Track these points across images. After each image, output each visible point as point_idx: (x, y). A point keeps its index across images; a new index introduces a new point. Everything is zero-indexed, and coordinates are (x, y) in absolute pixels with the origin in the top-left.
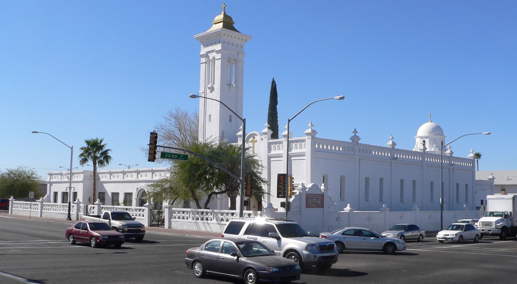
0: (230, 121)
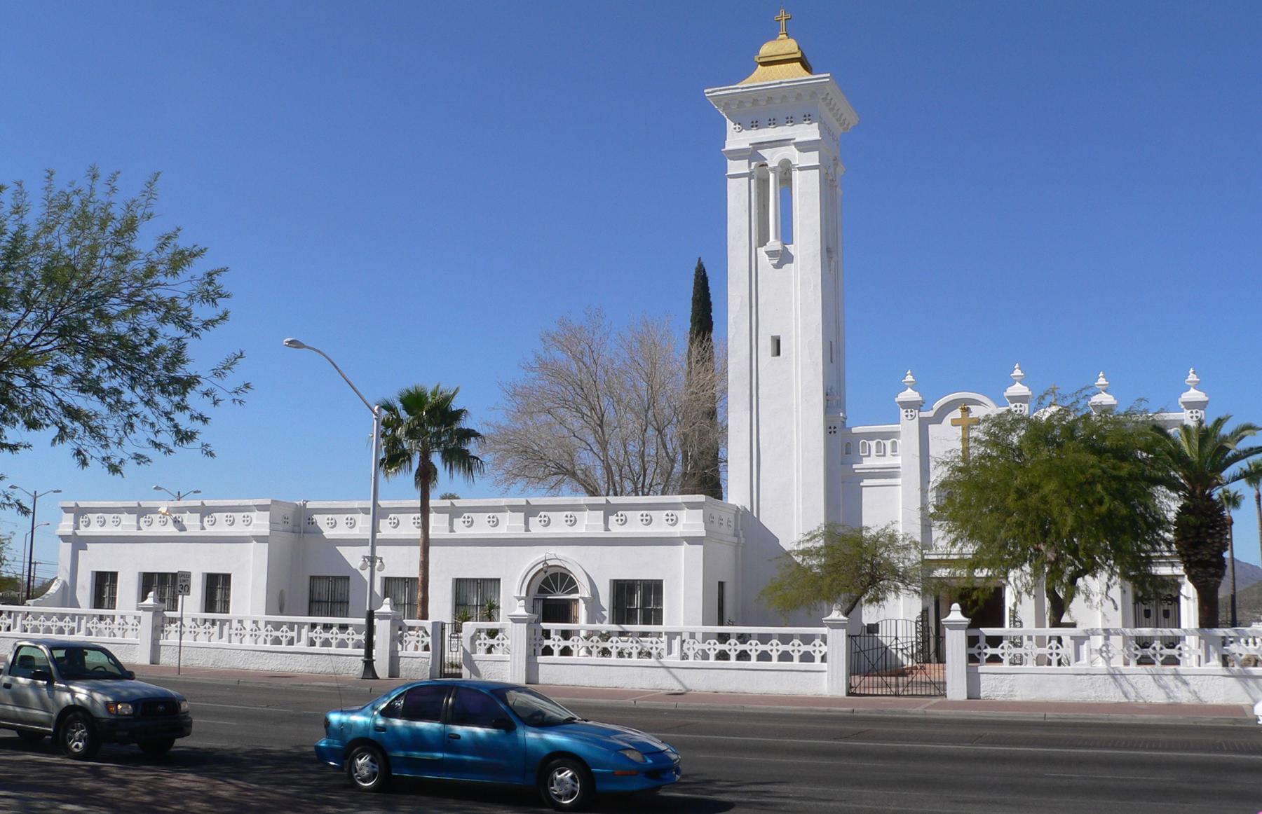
0: (832, 361)
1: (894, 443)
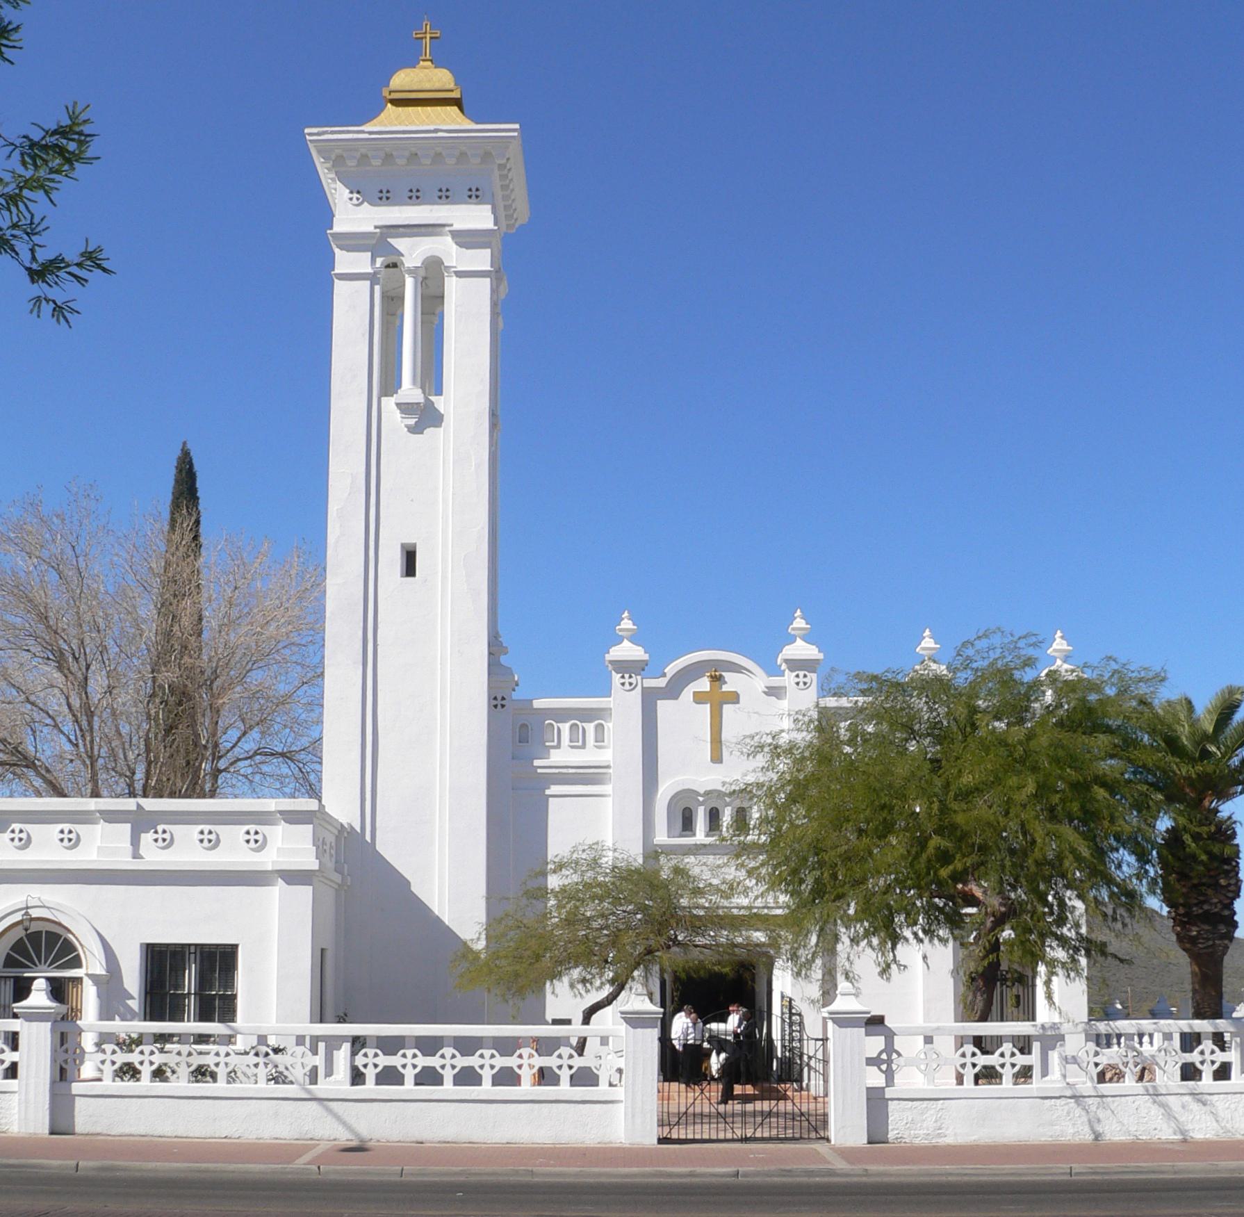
1: (600, 728)
